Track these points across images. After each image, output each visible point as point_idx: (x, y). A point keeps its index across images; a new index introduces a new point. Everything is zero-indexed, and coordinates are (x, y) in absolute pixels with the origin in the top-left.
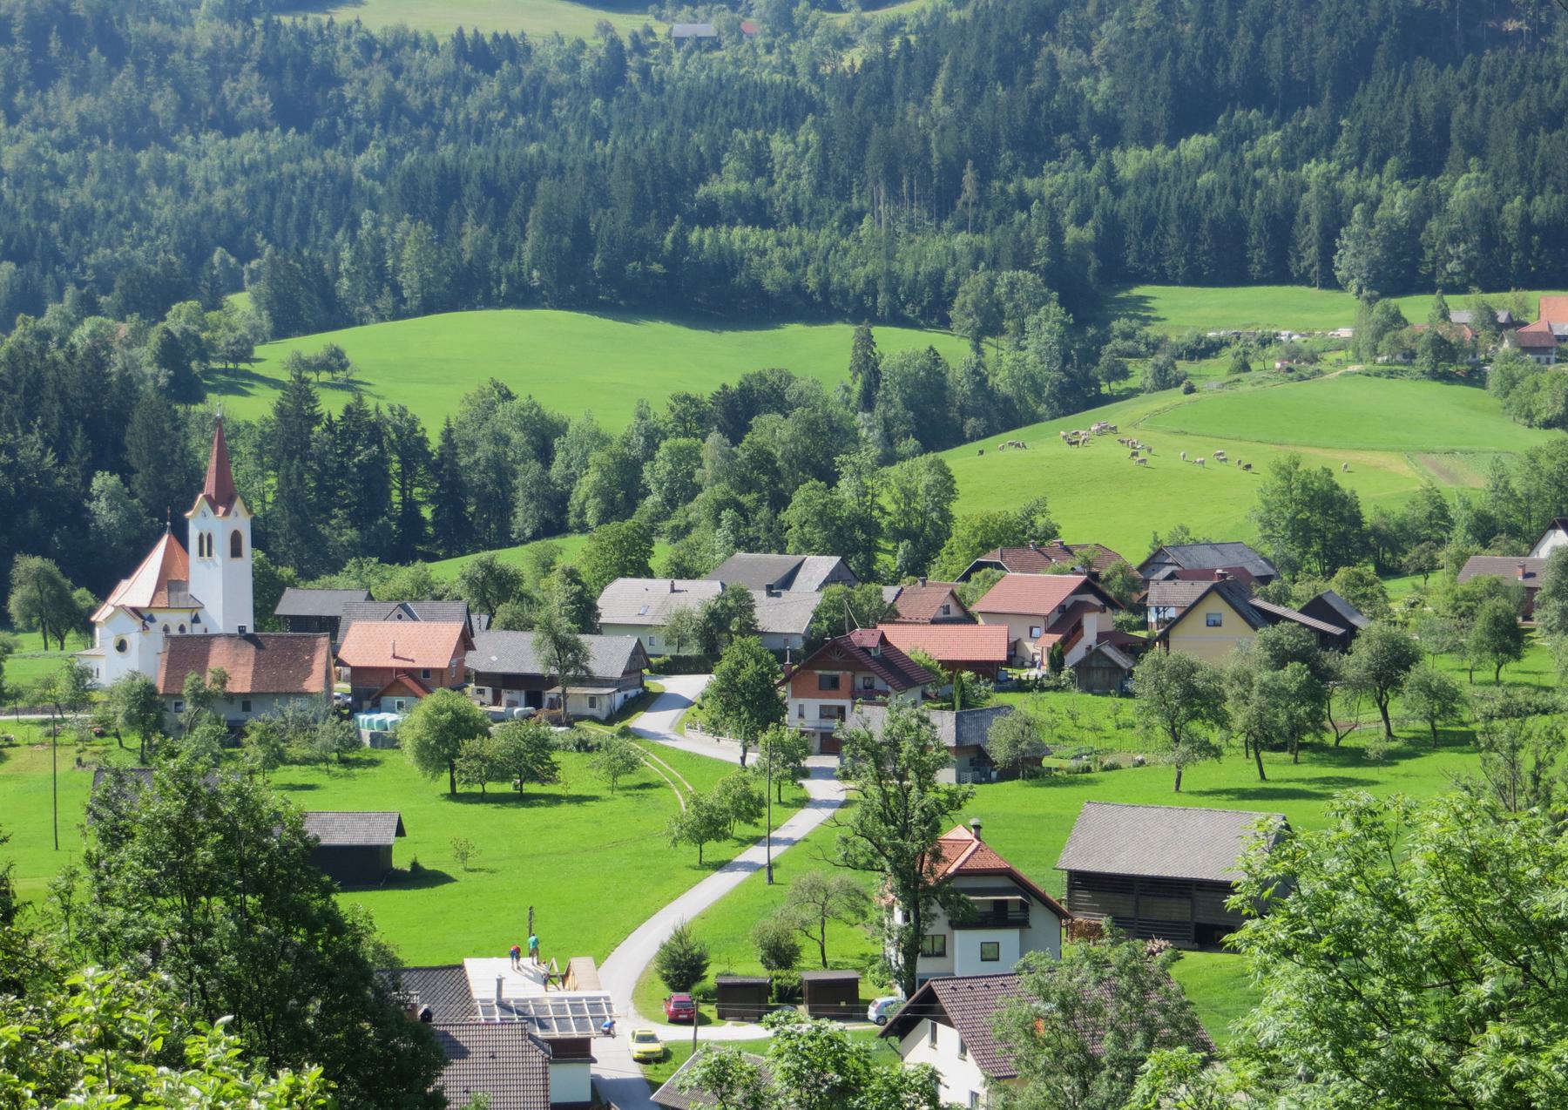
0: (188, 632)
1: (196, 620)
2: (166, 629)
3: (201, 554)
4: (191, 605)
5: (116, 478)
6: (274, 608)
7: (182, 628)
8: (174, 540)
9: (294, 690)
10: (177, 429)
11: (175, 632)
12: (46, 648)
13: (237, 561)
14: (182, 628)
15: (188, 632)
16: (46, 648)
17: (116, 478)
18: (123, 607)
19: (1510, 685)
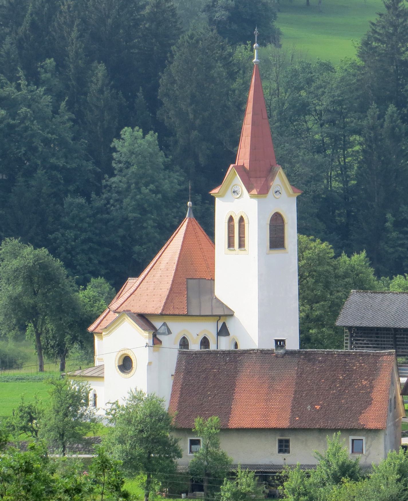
0: (213, 347)
1: (223, 331)
2: (184, 343)
3: (231, 244)
4: (218, 312)
5: (151, 137)
6: (336, 315)
7: (205, 342)
8: (195, 223)
9: (354, 425)
10: (232, 76)
11: (195, 346)
12: (41, 369)
13: (277, 254)
14: (205, 342)
15: (213, 347)
16: (41, 369)
17: (151, 137)
18: (128, 313)
19: (40, 380)
